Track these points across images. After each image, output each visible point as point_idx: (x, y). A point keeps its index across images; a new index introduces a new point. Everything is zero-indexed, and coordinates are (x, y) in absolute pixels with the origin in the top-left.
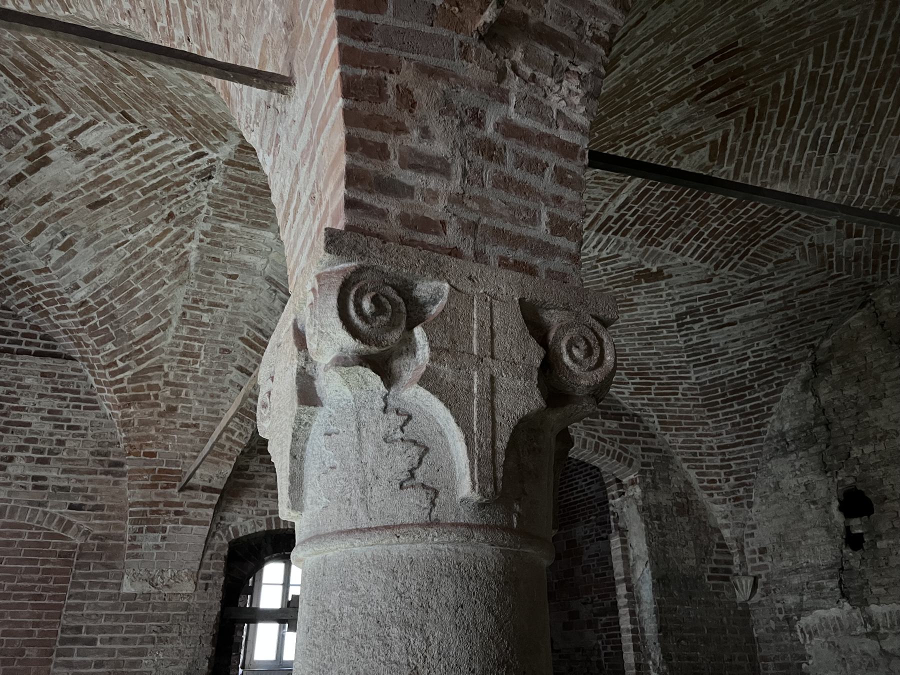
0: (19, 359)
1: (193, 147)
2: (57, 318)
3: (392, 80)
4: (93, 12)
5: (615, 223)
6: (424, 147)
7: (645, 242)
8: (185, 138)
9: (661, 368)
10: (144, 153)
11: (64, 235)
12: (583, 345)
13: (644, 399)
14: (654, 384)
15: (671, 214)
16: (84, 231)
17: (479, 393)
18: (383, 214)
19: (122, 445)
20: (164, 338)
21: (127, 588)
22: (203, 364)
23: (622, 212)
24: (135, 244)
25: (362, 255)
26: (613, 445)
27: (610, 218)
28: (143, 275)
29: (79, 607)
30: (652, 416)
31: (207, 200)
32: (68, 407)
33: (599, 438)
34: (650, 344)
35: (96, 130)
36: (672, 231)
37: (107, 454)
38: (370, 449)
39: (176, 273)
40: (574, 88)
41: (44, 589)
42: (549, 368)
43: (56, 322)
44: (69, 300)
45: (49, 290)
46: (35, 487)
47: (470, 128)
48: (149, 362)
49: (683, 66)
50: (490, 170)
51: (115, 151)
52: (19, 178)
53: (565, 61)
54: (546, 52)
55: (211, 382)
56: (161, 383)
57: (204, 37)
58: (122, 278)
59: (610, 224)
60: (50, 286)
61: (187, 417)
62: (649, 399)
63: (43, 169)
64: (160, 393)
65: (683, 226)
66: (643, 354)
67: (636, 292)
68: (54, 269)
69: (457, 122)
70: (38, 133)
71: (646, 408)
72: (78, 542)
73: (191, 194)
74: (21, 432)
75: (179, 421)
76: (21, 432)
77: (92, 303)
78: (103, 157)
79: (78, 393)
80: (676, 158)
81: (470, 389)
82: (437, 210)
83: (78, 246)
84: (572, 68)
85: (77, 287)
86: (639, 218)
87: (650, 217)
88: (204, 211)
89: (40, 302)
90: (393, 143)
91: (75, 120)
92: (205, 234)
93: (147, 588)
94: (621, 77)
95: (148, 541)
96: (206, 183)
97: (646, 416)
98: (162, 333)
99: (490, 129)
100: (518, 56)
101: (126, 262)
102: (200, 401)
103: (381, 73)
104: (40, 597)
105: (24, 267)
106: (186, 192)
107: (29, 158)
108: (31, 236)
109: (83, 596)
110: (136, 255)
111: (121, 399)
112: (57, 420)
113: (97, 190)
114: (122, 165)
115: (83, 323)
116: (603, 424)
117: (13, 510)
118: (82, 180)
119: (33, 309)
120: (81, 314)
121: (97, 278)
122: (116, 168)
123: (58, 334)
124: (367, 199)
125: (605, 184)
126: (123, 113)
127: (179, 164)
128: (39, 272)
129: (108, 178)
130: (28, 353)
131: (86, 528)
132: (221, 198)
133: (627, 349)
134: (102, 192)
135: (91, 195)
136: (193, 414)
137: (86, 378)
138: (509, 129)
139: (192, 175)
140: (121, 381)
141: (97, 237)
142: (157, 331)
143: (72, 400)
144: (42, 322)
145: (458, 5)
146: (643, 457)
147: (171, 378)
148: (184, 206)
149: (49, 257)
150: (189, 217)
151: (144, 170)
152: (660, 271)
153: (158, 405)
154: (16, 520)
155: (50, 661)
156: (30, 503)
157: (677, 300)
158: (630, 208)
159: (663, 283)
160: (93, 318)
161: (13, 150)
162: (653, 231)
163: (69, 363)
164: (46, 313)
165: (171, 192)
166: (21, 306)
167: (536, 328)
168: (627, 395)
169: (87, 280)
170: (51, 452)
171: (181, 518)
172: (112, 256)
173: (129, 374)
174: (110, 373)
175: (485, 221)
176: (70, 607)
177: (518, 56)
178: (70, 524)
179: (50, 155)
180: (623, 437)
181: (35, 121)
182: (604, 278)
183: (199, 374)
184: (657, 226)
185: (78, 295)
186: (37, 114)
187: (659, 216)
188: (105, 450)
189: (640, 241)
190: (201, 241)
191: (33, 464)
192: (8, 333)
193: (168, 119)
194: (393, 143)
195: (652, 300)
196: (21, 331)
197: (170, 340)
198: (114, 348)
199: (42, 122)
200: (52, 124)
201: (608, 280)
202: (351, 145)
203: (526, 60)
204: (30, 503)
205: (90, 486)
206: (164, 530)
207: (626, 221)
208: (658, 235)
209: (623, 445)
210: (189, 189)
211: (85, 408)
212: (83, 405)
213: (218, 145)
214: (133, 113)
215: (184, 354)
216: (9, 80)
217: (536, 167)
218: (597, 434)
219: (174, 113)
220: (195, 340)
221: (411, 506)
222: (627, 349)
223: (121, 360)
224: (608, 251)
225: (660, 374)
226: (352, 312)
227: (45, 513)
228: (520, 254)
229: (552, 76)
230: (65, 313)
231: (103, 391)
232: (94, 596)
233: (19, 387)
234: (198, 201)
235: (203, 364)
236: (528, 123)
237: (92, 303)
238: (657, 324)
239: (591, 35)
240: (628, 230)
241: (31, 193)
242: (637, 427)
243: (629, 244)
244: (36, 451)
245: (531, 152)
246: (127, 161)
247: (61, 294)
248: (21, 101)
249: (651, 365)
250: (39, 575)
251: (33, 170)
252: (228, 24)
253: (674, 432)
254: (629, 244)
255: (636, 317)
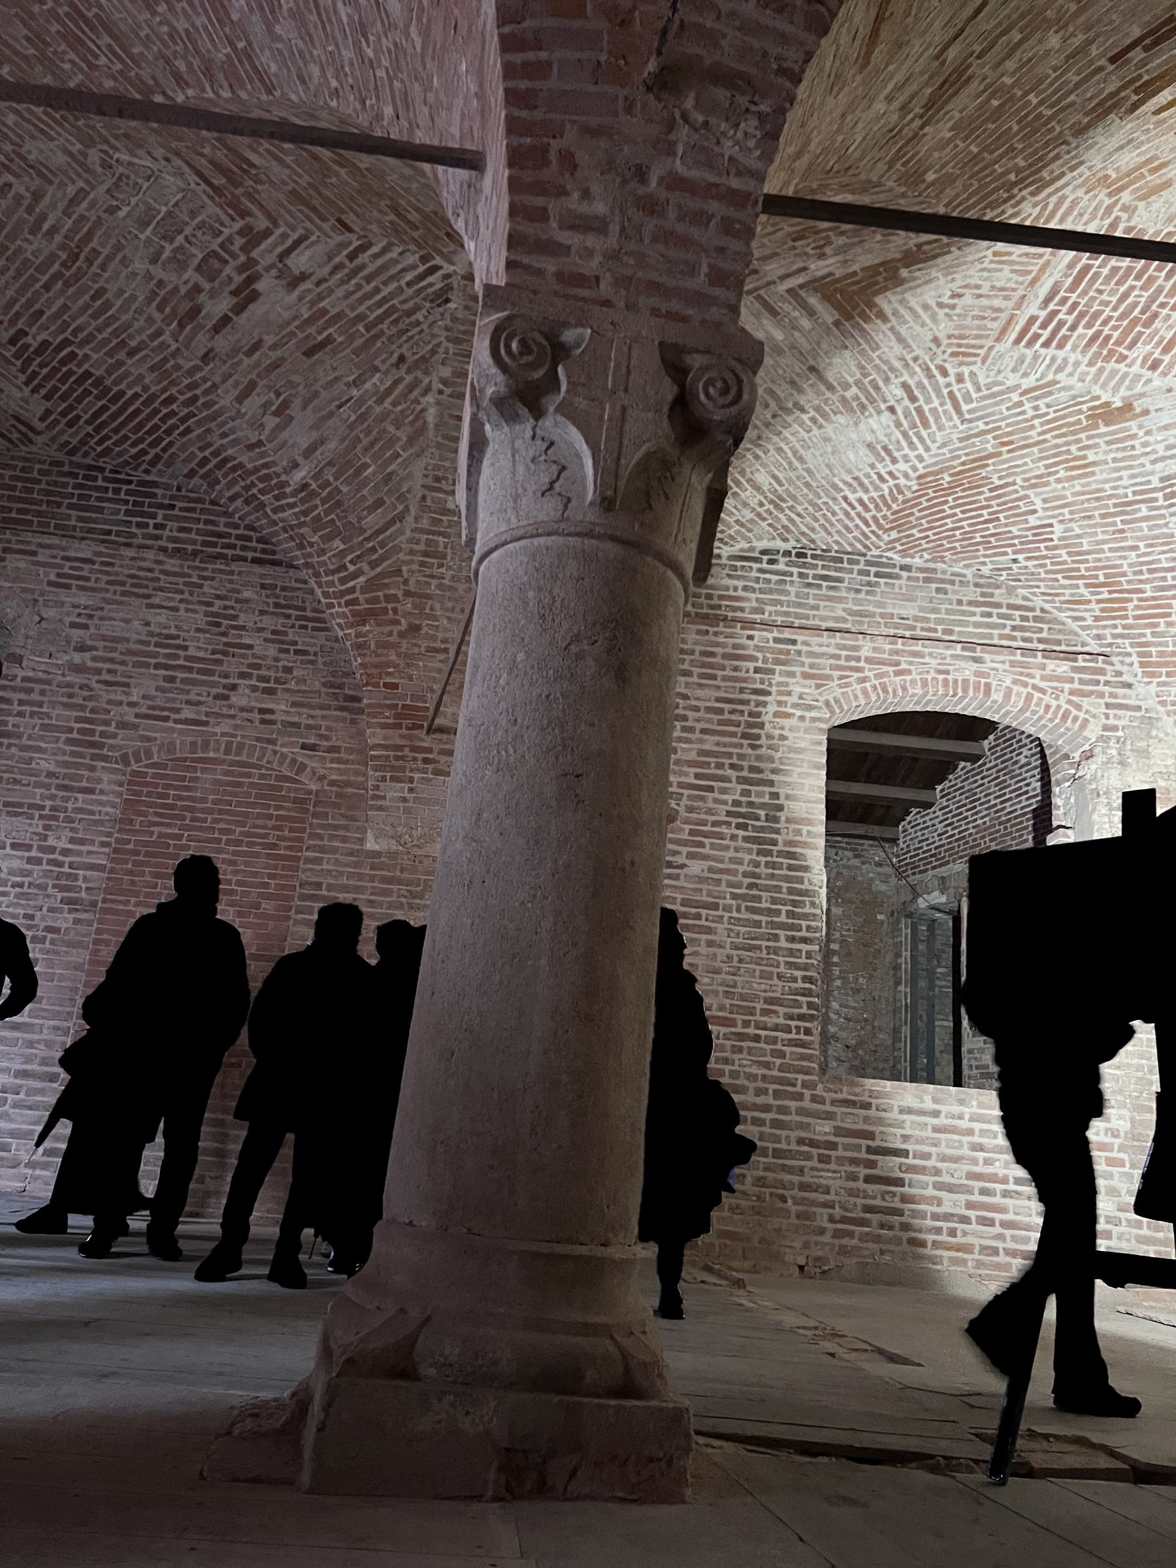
0: (235, 567)
1: (424, 259)
2: (275, 511)
3: (555, 144)
4: (297, 93)
5: (1044, 326)
6: (584, 208)
7: (1097, 355)
8: (413, 247)
9: (1141, 573)
10: (365, 273)
11: (278, 395)
12: (719, 385)
13: (1115, 626)
14: (1131, 600)
15: (1135, 304)
16: (300, 388)
17: (610, 419)
18: (540, 272)
19: (358, 676)
20: (401, 532)
21: (371, 845)
22: (450, 568)
23: (1052, 307)
24: (361, 401)
25: (514, 305)
26: (1057, 698)
27: (1032, 320)
28: (372, 444)
29: (318, 861)
30: (1129, 655)
31: (445, 333)
32: (293, 626)
33: (1035, 687)
34: (1122, 531)
35: (307, 248)
36: (1141, 334)
37: (341, 686)
38: (521, 469)
39: (411, 441)
40: (751, 130)
41: (279, 838)
42: (682, 404)
43: (274, 517)
44: (287, 483)
45: (264, 471)
46: (263, 721)
47: (633, 184)
48: (385, 564)
49: (1091, 62)
50: (650, 225)
51: (332, 273)
52: (225, 320)
53: (743, 101)
54: (721, 94)
55: (461, 591)
56: (400, 594)
57: (411, 114)
58: (348, 450)
59: (1035, 328)
60: (266, 466)
61: (433, 638)
62: (1124, 627)
63: (251, 306)
64: (399, 606)
65: (1157, 323)
66: (1111, 550)
67: (1090, 442)
68: (269, 442)
69: (618, 180)
70: (243, 258)
71: (1119, 641)
72: (313, 787)
73: (424, 326)
74: (243, 656)
75: (424, 644)
76: (243, 656)
77: (314, 486)
78: (318, 284)
79: (304, 609)
80: (1124, 208)
81: (601, 417)
82: (592, 266)
83: (294, 410)
84: (753, 108)
85: (296, 465)
86: (1082, 315)
87: (1098, 314)
88: (441, 350)
89: (255, 491)
90: (553, 207)
91: (284, 236)
92: (445, 382)
93: (394, 846)
94: (984, 91)
95: (393, 791)
96: (441, 309)
97: (1119, 654)
98: (398, 525)
99: (653, 183)
100: (689, 103)
101: (351, 427)
102: (449, 618)
103: (545, 140)
104: (274, 846)
105: (235, 442)
106: (418, 323)
107: (235, 293)
108: (240, 399)
109: (322, 849)
110: (362, 418)
111: (355, 614)
112: (282, 642)
113: (312, 330)
114: (340, 293)
115: (305, 513)
116: (1043, 667)
117: (241, 746)
118: (295, 318)
119: (247, 502)
120: (303, 501)
121: (319, 451)
122: (333, 297)
123: (276, 533)
124: (526, 260)
125: (1012, 263)
126: (339, 220)
127: (409, 284)
128: (251, 447)
129: (324, 311)
130: (244, 559)
131: (322, 772)
132: (462, 328)
133: (1084, 541)
134: (319, 333)
135: (307, 337)
136: (440, 635)
137: (312, 592)
138: (675, 182)
139: (424, 299)
140: (352, 590)
141: (316, 395)
142: (392, 522)
143: (298, 618)
144: (258, 519)
145: (624, 57)
146: (1107, 717)
147: (412, 586)
148: (417, 344)
149: (262, 426)
150: (424, 359)
151: (368, 296)
152: (1128, 407)
153: (398, 623)
154: (244, 758)
155: (288, 918)
156: (258, 739)
157: (1161, 453)
158: (1064, 300)
159: (1133, 424)
160: (316, 507)
161: (217, 283)
162: (1108, 337)
163: (292, 572)
164: (262, 505)
165: (401, 326)
166: (232, 499)
167: (676, 369)
168: (1089, 622)
169: (308, 453)
170: (277, 681)
171: (430, 767)
172: (331, 422)
173: (362, 579)
174: (340, 579)
175: (640, 274)
176: (308, 860)
177: (689, 103)
178: (303, 766)
179: (260, 286)
180: (1076, 685)
181: (239, 242)
182: (1036, 422)
183: (446, 581)
184: (1115, 328)
185: (299, 476)
186: (241, 233)
187: (1115, 309)
188: (339, 681)
189: (1089, 355)
190: (440, 392)
191: (258, 694)
192: (220, 535)
193: (391, 222)
194: (553, 207)
195: (1120, 455)
196: (234, 532)
197: (408, 534)
198: (342, 547)
199: (248, 242)
200: (259, 244)
201: (1042, 424)
202: (513, 211)
203: (697, 106)
204: (258, 739)
205: (324, 723)
206: (411, 780)
207: (1061, 324)
208: (1119, 343)
209: (1074, 698)
210: (421, 319)
211: (314, 629)
212: (311, 625)
213: (454, 252)
214: (350, 218)
215: (426, 554)
216: (208, 189)
217: (701, 218)
218: (1031, 681)
219: (398, 214)
220: (440, 534)
221: (548, 509)
222: (1084, 541)
223: (351, 562)
224: (1038, 375)
225: (1141, 581)
226: (503, 352)
227: (275, 752)
228: (675, 306)
229: (727, 119)
230: (284, 502)
231: (331, 606)
232: (334, 850)
233: (237, 601)
234: (434, 336)
235: (450, 568)
236: (695, 174)
237: (314, 486)
238: (1131, 498)
239: (775, 67)
240: (1066, 338)
241: (239, 341)
242: (1102, 672)
243: (1071, 361)
244: (261, 679)
245: (696, 204)
246: (345, 287)
247: (278, 475)
248: (224, 217)
249: (1125, 568)
250: (273, 822)
251: (239, 309)
252: (431, 97)
253: (1163, 678)
254: (1071, 361)
255: (1094, 486)
